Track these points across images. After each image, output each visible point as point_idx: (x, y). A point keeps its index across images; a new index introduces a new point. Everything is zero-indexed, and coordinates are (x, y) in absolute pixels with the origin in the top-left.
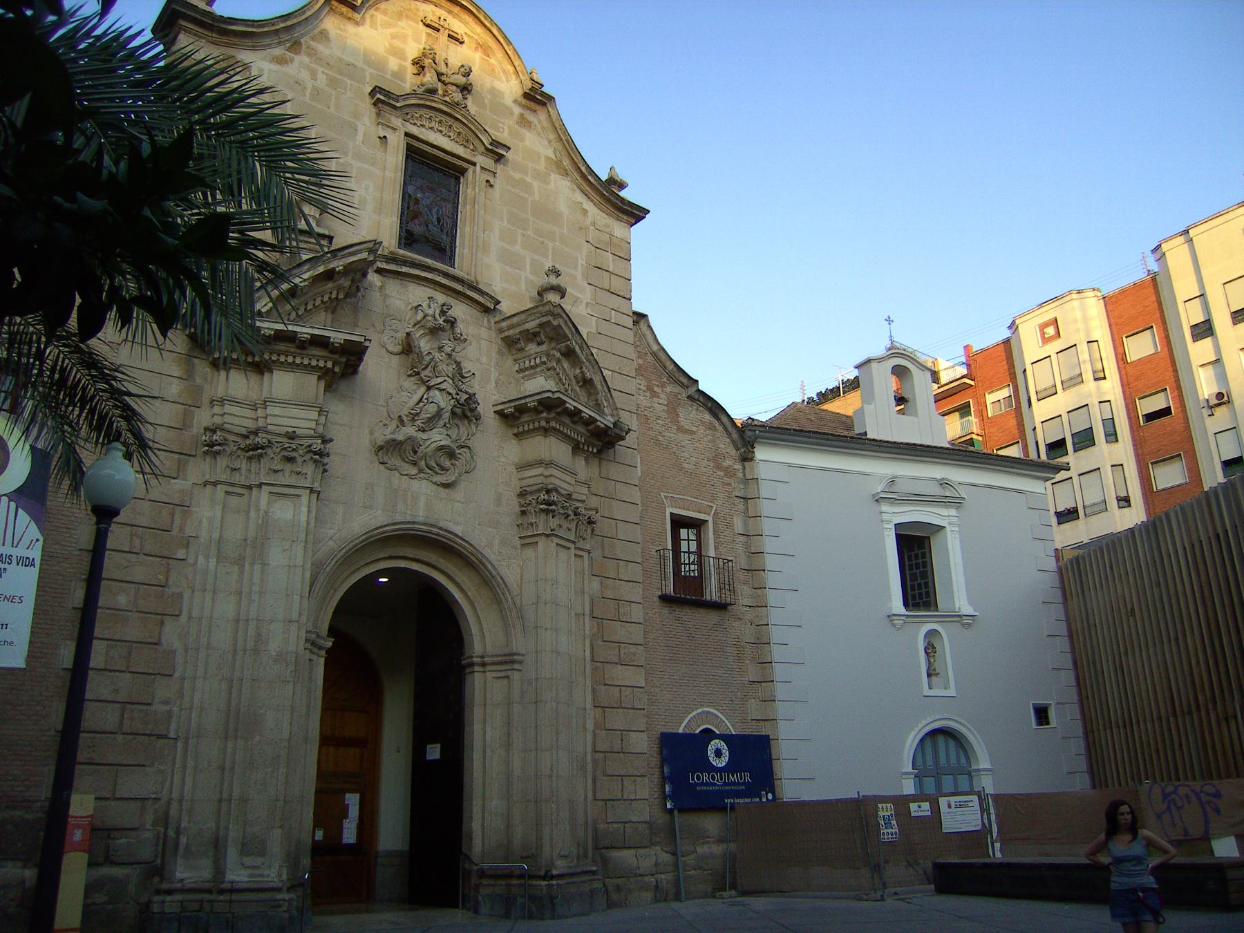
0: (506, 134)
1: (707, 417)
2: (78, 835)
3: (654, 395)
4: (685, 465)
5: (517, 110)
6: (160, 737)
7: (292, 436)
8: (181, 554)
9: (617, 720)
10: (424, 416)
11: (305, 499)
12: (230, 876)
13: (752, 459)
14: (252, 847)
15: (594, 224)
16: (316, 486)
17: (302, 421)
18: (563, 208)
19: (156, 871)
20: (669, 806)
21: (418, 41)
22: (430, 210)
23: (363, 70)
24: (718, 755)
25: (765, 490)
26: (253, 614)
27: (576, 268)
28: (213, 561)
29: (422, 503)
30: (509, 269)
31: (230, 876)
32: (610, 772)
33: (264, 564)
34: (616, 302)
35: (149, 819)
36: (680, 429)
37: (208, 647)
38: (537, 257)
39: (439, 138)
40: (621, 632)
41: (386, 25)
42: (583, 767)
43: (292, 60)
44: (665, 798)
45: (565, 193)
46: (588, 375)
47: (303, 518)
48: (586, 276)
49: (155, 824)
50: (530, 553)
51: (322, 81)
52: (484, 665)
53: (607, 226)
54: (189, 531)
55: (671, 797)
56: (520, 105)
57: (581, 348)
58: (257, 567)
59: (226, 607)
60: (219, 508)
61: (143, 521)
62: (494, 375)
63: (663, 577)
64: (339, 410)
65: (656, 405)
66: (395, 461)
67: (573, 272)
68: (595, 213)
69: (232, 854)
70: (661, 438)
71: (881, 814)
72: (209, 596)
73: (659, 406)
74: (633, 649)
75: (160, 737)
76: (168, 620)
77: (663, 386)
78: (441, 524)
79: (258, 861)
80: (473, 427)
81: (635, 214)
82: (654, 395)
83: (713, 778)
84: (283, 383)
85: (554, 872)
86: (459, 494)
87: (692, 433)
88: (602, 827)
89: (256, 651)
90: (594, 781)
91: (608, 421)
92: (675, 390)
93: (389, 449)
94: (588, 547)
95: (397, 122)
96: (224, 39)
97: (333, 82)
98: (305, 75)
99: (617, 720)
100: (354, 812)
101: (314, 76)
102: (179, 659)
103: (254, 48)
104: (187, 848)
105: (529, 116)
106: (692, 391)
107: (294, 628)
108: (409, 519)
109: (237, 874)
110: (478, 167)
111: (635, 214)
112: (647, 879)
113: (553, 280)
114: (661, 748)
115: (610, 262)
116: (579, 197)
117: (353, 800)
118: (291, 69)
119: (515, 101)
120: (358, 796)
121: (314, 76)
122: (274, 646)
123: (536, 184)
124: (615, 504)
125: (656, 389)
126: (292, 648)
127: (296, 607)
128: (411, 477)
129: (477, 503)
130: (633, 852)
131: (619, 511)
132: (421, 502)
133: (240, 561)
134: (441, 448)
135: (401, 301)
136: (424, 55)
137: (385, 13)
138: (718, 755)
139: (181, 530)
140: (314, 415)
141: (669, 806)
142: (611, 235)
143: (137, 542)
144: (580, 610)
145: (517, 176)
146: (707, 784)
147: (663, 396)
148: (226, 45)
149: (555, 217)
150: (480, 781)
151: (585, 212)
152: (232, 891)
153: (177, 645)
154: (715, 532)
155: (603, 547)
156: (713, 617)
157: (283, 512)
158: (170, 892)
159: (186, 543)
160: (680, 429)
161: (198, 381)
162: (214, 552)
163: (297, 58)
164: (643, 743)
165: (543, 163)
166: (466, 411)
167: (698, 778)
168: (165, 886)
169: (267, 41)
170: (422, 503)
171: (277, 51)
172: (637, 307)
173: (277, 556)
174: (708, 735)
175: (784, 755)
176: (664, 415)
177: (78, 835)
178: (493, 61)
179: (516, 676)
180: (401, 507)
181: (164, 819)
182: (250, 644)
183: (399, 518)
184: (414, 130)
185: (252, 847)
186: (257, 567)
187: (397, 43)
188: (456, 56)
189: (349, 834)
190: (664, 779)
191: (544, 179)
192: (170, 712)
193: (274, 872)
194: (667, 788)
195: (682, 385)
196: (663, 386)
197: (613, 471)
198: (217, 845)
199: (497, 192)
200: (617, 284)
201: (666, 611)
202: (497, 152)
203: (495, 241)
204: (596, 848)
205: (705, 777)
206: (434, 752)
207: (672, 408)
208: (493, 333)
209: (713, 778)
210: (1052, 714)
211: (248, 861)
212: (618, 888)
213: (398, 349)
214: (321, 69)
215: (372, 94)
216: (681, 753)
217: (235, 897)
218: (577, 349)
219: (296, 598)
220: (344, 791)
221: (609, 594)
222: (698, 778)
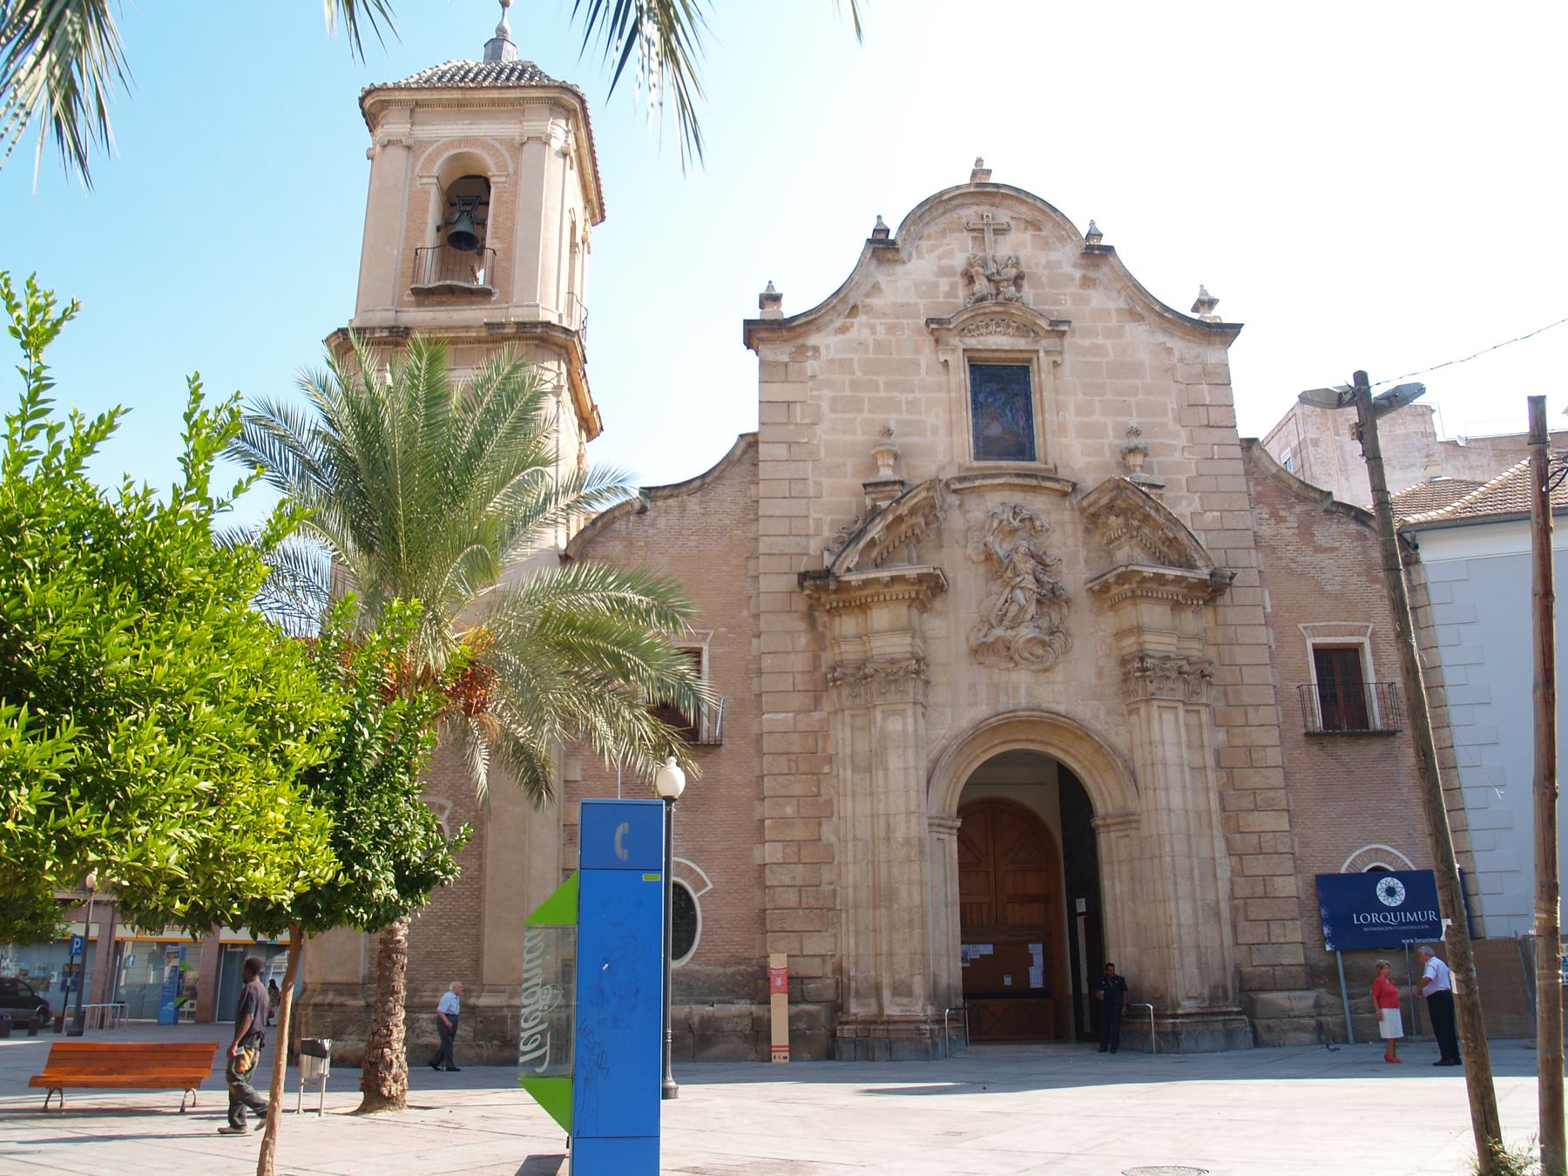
0: (1069, 304)
1: (1353, 527)
2: (779, 982)
4: (1329, 588)
5: (1078, 274)
6: (829, 909)
7: (892, 662)
8: (826, 769)
9: (1258, 866)
10: (1010, 614)
11: (910, 712)
12: (887, 1012)
13: (1417, 561)
14: (903, 990)
15: (1181, 360)
16: (920, 698)
17: (895, 646)
18: (1144, 356)
19: (837, 1007)
20: (1328, 948)
21: (964, 250)
24: (1392, 894)
25: (1436, 594)
26: (881, 811)
27: (1165, 414)
28: (849, 772)
29: (1022, 691)
30: (1090, 442)
31: (887, 1012)
32: (1252, 916)
33: (886, 769)
34: (1217, 435)
35: (829, 968)
36: (1318, 549)
37: (855, 839)
39: (999, 342)
40: (1255, 779)
41: (931, 250)
42: (1217, 914)
44: (1324, 940)
45: (1141, 338)
46: (1170, 535)
47: (910, 728)
48: (1179, 420)
49: (834, 972)
50: (1135, 719)
51: (881, 329)
52: (1107, 826)
53: (1198, 356)
54: (831, 751)
55: (1331, 940)
56: (1081, 266)
57: (1157, 510)
58: (880, 773)
59: (864, 807)
60: (848, 729)
61: (795, 749)
62: (1082, 554)
63: (1306, 711)
64: (934, 625)
65: (1284, 531)
66: (991, 660)
67: (1162, 420)
68: (1179, 345)
69: (886, 994)
70: (1293, 565)
72: (849, 800)
73: (1289, 529)
74: (1271, 794)
75: (829, 909)
76: (824, 821)
77: (1290, 507)
78: (1044, 706)
79: (905, 1000)
80: (1065, 610)
81: (1228, 332)
82: (1282, 520)
83: (1385, 918)
84: (880, 617)
85: (1180, 1012)
86: (1059, 674)
87: (1333, 549)
88: (1246, 969)
89: (888, 839)
90: (1234, 926)
91: (1204, 573)
92: (1306, 508)
93: (981, 652)
94: (1204, 700)
95: (955, 341)
97: (891, 329)
98: (866, 333)
99: (1258, 866)
100: (1038, 960)
102: (836, 849)
103: (818, 330)
104: (857, 991)
105: (1092, 274)
106: (1327, 504)
107: (913, 818)
108: (1011, 707)
109: (892, 1010)
110: (1042, 354)
111: (1228, 332)
113: (1135, 442)
115: (1206, 394)
116: (1161, 338)
117: (1036, 950)
118: (852, 334)
119: (1074, 265)
120: (1040, 947)
122: (900, 834)
123: (1108, 343)
124: (1237, 649)
125: (1281, 513)
126: (914, 833)
127: (913, 801)
128: (1007, 669)
129: (1071, 687)
130: (1285, 994)
131: (1242, 656)
132: (1024, 689)
133: (869, 770)
134: (1030, 640)
135: (973, 516)
136: (971, 265)
137: (929, 237)
138: (1392, 894)
139: (824, 750)
140: (908, 640)
141: (1328, 948)
143: (793, 765)
144: (1198, 763)
145: (1087, 342)
146: (1377, 924)
148: (795, 338)
149: (1134, 369)
151: (1170, 351)
152: (889, 1022)
153: (833, 839)
154: (1374, 653)
155: (1226, 695)
156: (1378, 748)
157: (894, 725)
158: (847, 1023)
159: (830, 760)
160: (1318, 549)
161: (820, 629)
162: (848, 762)
163: (856, 321)
164: (1290, 886)
165: (1114, 317)
166: (1050, 597)
167: (1365, 918)
168: (844, 1019)
169: (827, 318)
170: (1022, 691)
171: (839, 323)
172: (1244, 432)
173: (895, 762)
174: (1379, 873)
175: (1483, 889)
177: (779, 982)
178: (1044, 233)
179: (1133, 834)
180: (1003, 699)
181: (839, 970)
182: (882, 834)
183: (1001, 708)
184: (973, 342)
185: (903, 990)
186: (880, 773)
187: (945, 262)
188: (1004, 248)
189: (1036, 979)
190: (1323, 921)
191: (1118, 333)
192: (834, 891)
193: (919, 1008)
194: (1326, 931)
195: (1316, 501)
196: (1290, 507)
197: (1232, 615)
198: (877, 989)
199: (1066, 369)
200: (1216, 416)
201: (1315, 749)
202: (1058, 328)
203: (1072, 419)
204: (1242, 990)
205: (1374, 917)
207: (1305, 530)
208: (1077, 513)
209: (1385, 918)
211: (898, 1000)
212: (1269, 1029)
213: (982, 558)
214: (877, 322)
215: (927, 324)
216: (1342, 898)
218: (1153, 513)
219: (913, 794)
220: (1027, 943)
221: (1238, 742)
222: (1365, 918)
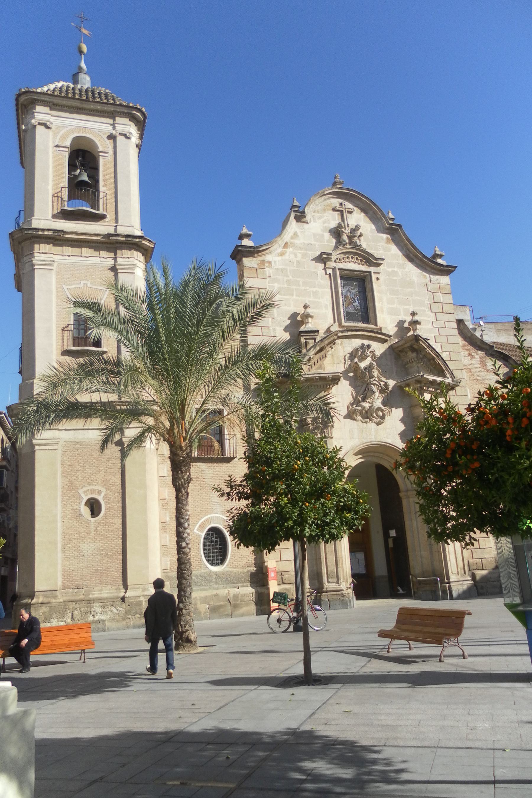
3: (473, 357)
22: (354, 299)
23: (315, 245)
38: (406, 307)
43: (286, 252)
70: (479, 378)
71: (196, 455)
96: (259, 254)
98: (292, 257)
101: (296, 256)
112: (495, 583)
114: (71, 418)
121: (296, 256)
125: (473, 354)
142: (439, 283)
145: (390, 270)
147: (476, 357)
150: (450, 666)
176: (479, 366)
206: (393, 533)
210: (86, 511)
217: (328, 593)
